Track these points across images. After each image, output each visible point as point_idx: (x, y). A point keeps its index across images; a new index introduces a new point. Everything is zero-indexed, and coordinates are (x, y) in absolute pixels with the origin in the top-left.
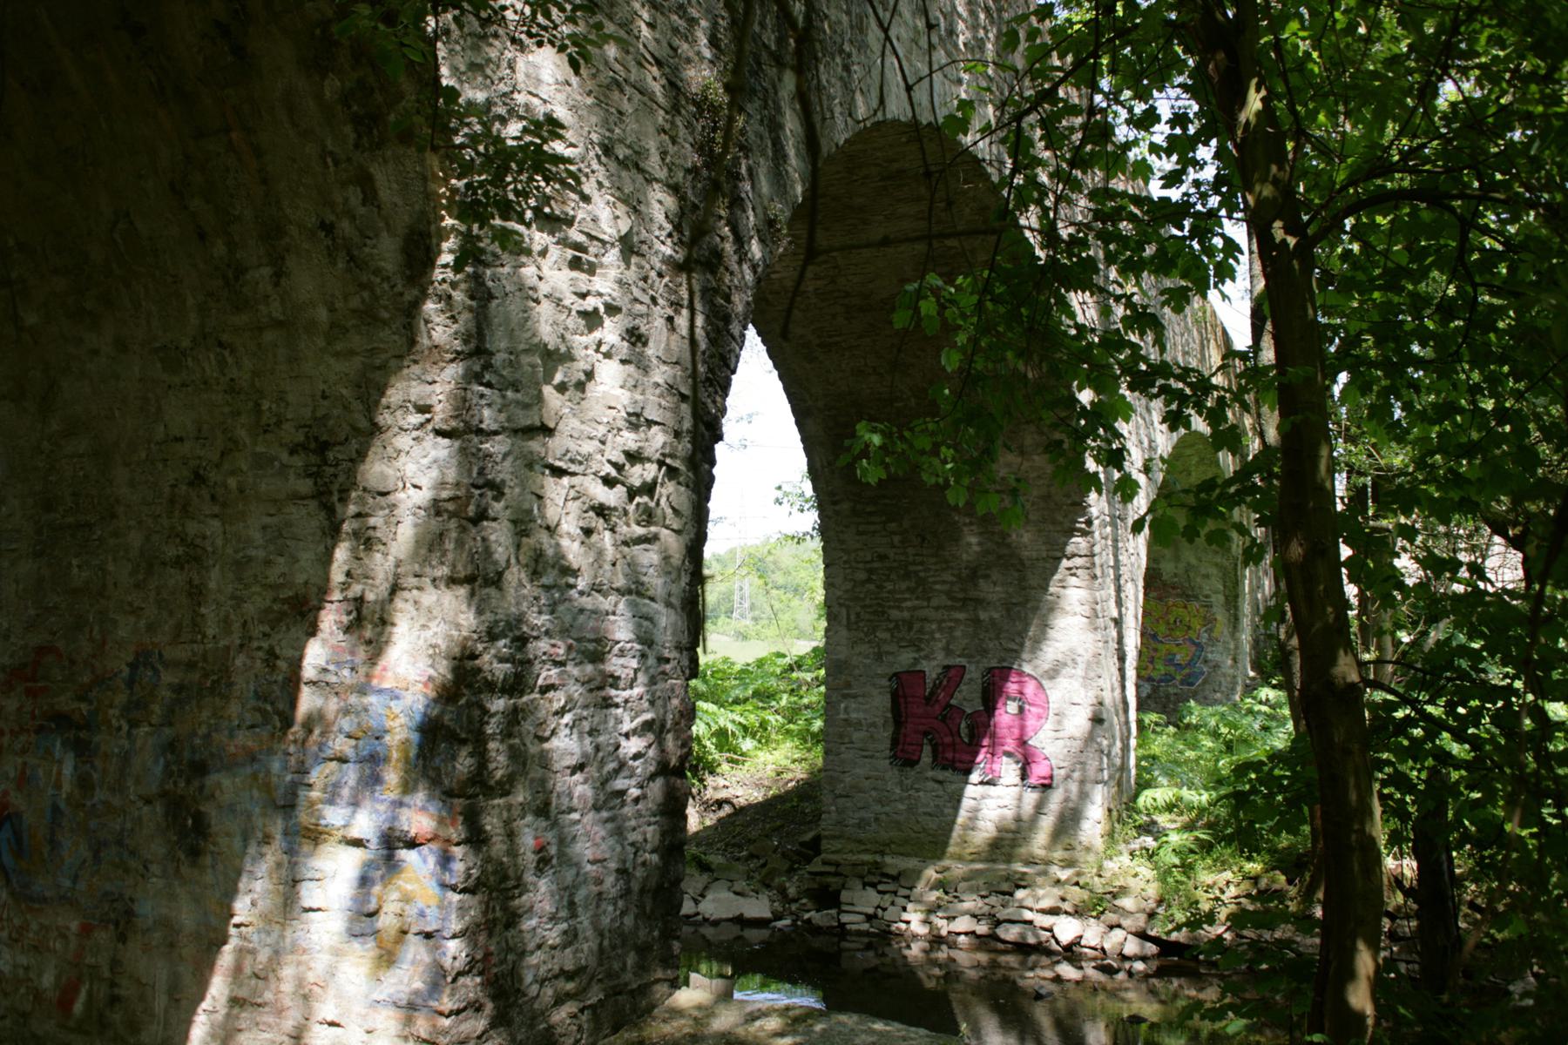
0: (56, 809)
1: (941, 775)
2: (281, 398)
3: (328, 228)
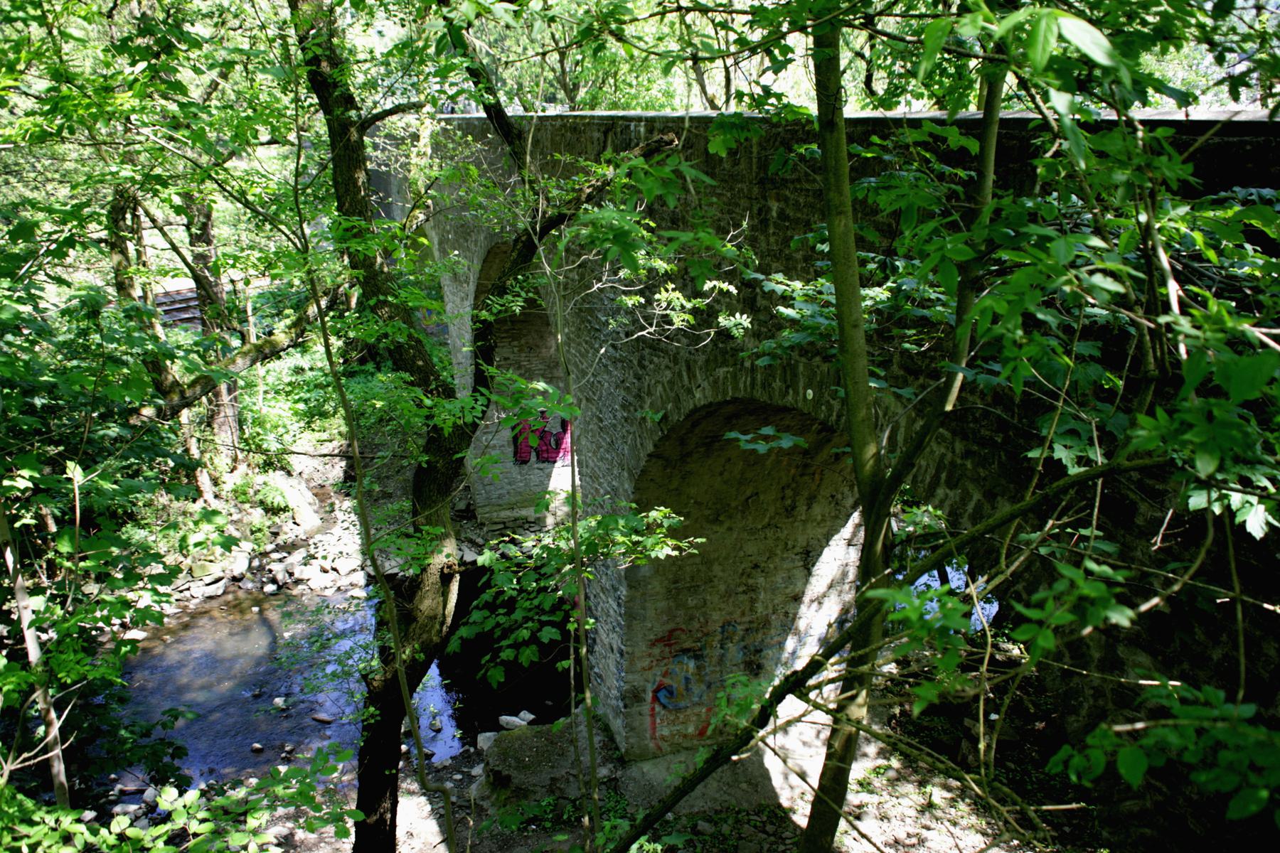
0: (687, 679)
1: (542, 466)
2: (796, 540)
3: (833, 497)
